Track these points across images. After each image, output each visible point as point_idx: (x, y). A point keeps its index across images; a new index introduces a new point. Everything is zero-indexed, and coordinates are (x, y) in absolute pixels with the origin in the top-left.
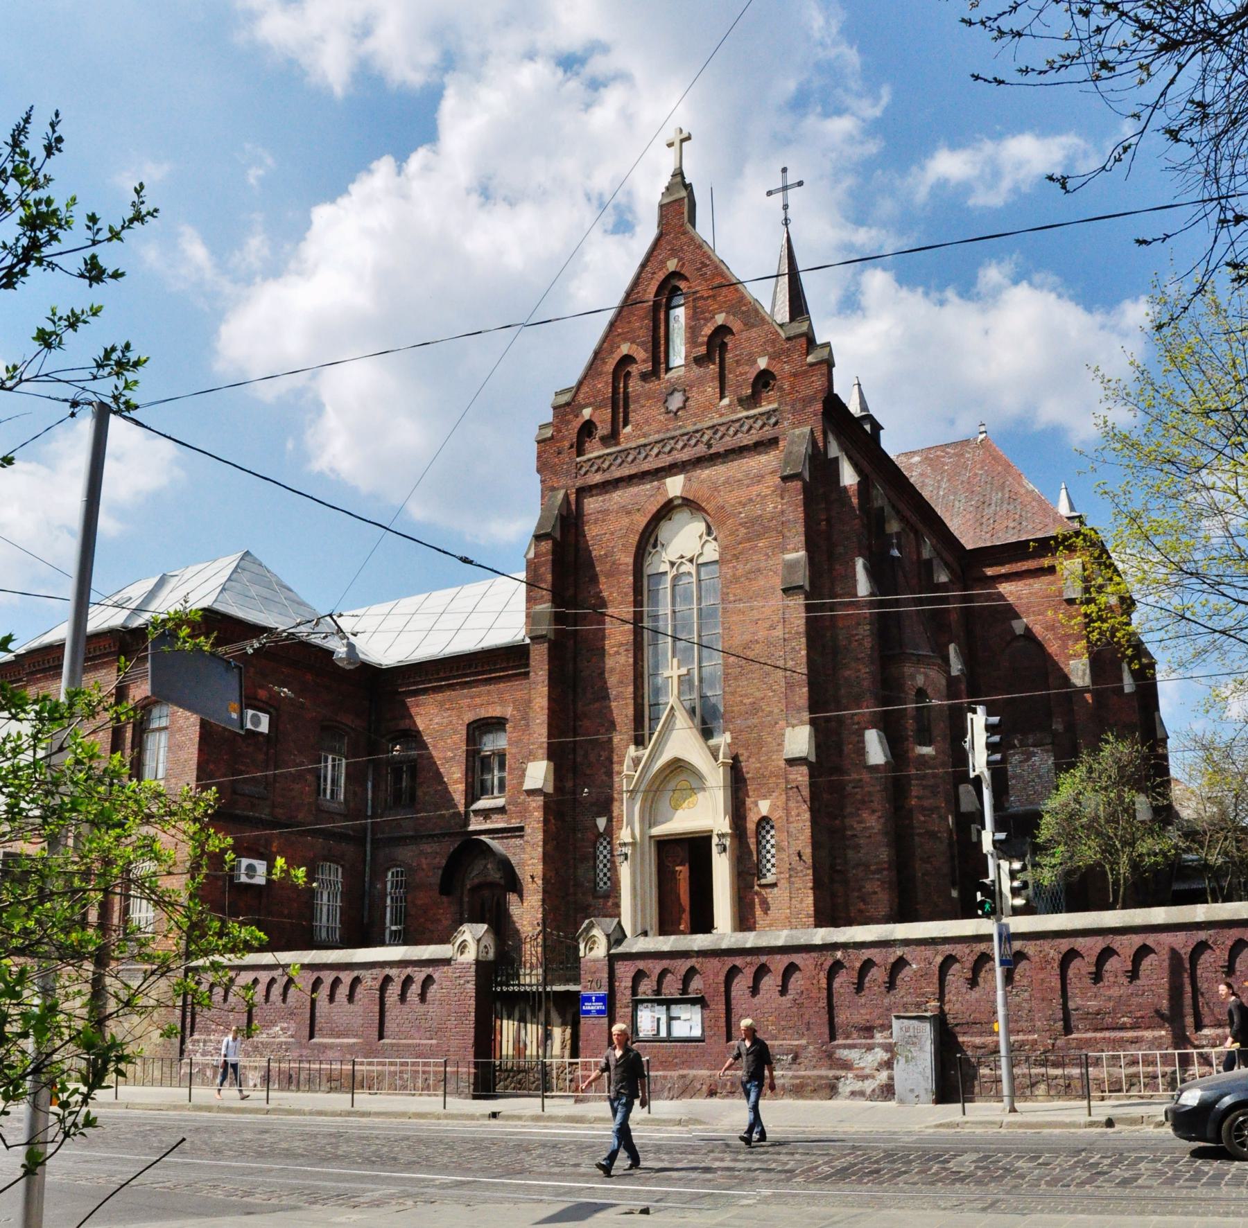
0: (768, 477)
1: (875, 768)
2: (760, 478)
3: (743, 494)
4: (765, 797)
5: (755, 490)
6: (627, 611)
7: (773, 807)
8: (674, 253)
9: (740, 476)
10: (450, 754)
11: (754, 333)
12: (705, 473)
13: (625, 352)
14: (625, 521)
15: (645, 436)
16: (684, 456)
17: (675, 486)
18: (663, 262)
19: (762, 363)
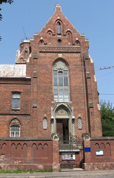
0: (78, 58)
1: (99, 110)
2: (77, 58)
3: (74, 60)
4: (79, 114)
5: (76, 60)
6: (83, 77)
7: (81, 115)
8: (59, 16)
9: (73, 57)
10: (7, 97)
11: (75, 34)
12: (66, 54)
13: (69, 30)
14: (50, 60)
15: (54, 45)
16: (63, 51)
17: (60, 55)
18: (57, 17)
19: (42, 38)
